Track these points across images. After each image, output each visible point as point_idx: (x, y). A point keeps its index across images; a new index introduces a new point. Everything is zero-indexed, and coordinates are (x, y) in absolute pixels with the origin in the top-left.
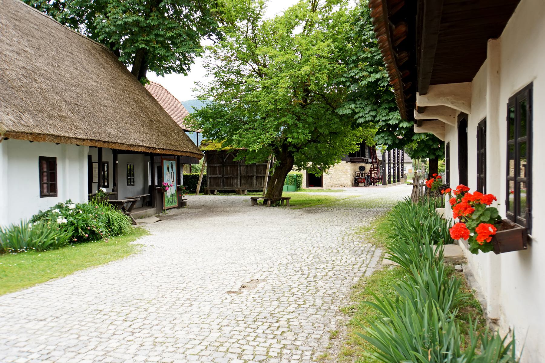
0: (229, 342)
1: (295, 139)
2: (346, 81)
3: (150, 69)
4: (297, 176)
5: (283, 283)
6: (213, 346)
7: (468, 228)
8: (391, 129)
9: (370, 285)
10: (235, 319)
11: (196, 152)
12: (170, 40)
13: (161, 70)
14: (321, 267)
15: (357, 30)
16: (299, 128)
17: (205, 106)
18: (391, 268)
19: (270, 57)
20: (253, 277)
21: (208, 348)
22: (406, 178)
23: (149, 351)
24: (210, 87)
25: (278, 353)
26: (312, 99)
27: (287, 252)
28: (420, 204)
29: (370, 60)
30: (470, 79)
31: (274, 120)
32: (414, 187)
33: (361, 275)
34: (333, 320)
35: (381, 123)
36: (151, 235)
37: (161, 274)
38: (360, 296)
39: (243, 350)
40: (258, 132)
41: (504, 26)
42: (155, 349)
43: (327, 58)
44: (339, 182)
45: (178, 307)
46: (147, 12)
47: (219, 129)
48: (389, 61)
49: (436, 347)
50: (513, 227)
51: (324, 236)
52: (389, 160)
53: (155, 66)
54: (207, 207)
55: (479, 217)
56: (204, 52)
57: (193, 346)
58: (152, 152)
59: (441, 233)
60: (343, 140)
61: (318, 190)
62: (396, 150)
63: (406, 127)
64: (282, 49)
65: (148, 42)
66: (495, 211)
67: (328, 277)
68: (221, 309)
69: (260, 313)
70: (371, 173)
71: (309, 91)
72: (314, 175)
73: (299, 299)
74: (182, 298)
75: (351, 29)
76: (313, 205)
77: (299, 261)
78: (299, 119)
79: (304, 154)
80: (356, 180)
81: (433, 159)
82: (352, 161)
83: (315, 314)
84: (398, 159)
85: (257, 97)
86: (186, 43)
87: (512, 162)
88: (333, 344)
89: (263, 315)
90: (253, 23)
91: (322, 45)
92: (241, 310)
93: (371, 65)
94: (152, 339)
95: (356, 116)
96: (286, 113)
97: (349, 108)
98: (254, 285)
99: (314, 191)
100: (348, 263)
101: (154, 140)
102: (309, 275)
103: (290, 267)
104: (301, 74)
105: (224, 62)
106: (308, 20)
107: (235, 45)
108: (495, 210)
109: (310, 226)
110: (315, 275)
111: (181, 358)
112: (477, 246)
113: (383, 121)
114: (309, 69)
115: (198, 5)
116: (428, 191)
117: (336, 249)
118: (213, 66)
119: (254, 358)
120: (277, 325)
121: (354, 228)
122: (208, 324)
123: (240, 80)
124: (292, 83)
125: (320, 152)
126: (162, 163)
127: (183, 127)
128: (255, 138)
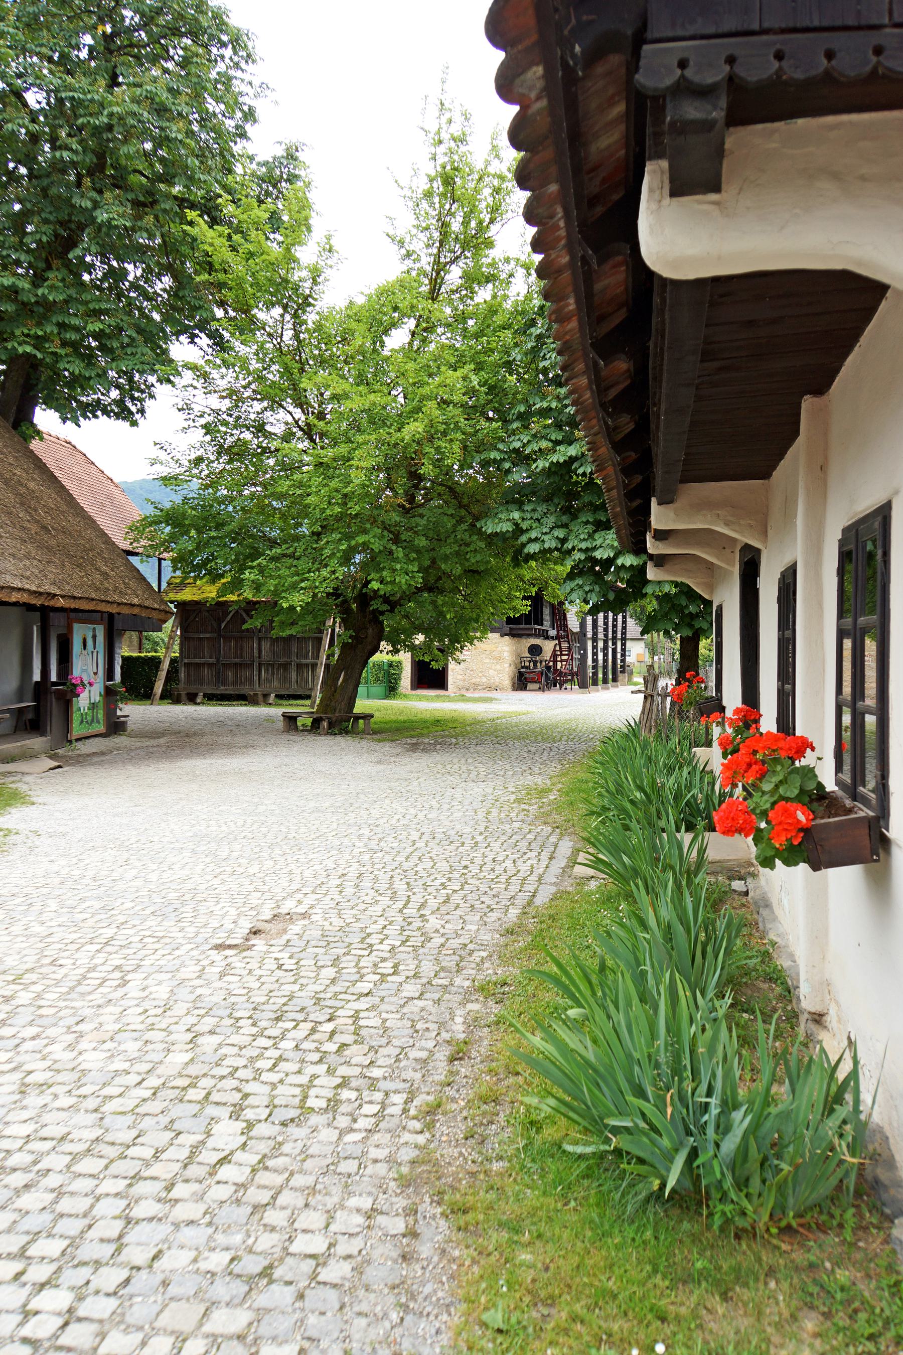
0: (213, 1077)
1: (387, 583)
2: (503, 460)
3: (44, 403)
4: (391, 665)
5: (348, 921)
6: (173, 1088)
7: (754, 810)
8: (597, 568)
9: (544, 926)
10: (230, 1016)
11: (156, 606)
12: (95, 339)
13: (73, 410)
14: (437, 883)
15: (529, 345)
16: (396, 560)
17: (178, 500)
18: (593, 884)
19: (335, 397)
20: (278, 907)
21: (158, 1095)
22: (631, 673)
23: (6, 1110)
24: (193, 457)
25: (329, 1100)
26: (426, 494)
27: (361, 844)
28: (658, 736)
29: (556, 415)
30: (765, 474)
31: (340, 540)
32: (646, 697)
33: (525, 903)
34: (458, 1012)
35: (578, 556)
36: (33, 804)
37: (53, 905)
38: (521, 953)
39: (246, 1096)
40: (303, 564)
41: (837, 371)
42: (25, 1102)
43: (462, 406)
44: (484, 680)
45: (90, 989)
46: (37, 268)
47: (212, 555)
48: (592, 431)
49: (685, 1084)
50: (850, 811)
51: (445, 807)
52: (595, 633)
53: (57, 399)
54: (177, 733)
55: (777, 786)
56: (179, 374)
57: (123, 1089)
58: (46, 604)
59: (702, 806)
60: (493, 588)
61: (437, 696)
62: (611, 615)
63: (631, 565)
64: (361, 380)
65: (39, 342)
66: (810, 775)
67: (452, 906)
68: (199, 991)
69: (291, 997)
70: (555, 662)
71: (420, 478)
72: (429, 663)
73: (384, 960)
74: (103, 964)
75: (516, 345)
76: (425, 731)
77: (389, 868)
78: (396, 540)
79: (406, 616)
80: (521, 675)
81: (688, 637)
82: (513, 634)
83: (419, 998)
84: (615, 632)
85: (300, 485)
86: (134, 350)
87: (848, 644)
88: (458, 1073)
89: (297, 1003)
90: (295, 316)
91: (453, 377)
92: (246, 991)
93: (558, 426)
94: (18, 1076)
95: (524, 538)
96: (368, 526)
97: (508, 520)
98: (281, 926)
99: (428, 699)
100: (497, 872)
101: (52, 576)
102: (408, 902)
103: (366, 883)
104: (403, 440)
105: (227, 401)
106: (420, 316)
107: (254, 365)
108: (809, 772)
109: (415, 783)
110: (422, 900)
111: (90, 1124)
112: (771, 853)
113: (580, 550)
114: (420, 430)
115: (164, 261)
116: (677, 709)
117: (473, 838)
118: (201, 409)
119: (270, 1115)
120: (329, 1027)
121: (514, 789)
122: (164, 1030)
123: (264, 445)
124: (381, 459)
125: (442, 614)
126: (70, 629)
127: (125, 545)
128: (296, 578)
